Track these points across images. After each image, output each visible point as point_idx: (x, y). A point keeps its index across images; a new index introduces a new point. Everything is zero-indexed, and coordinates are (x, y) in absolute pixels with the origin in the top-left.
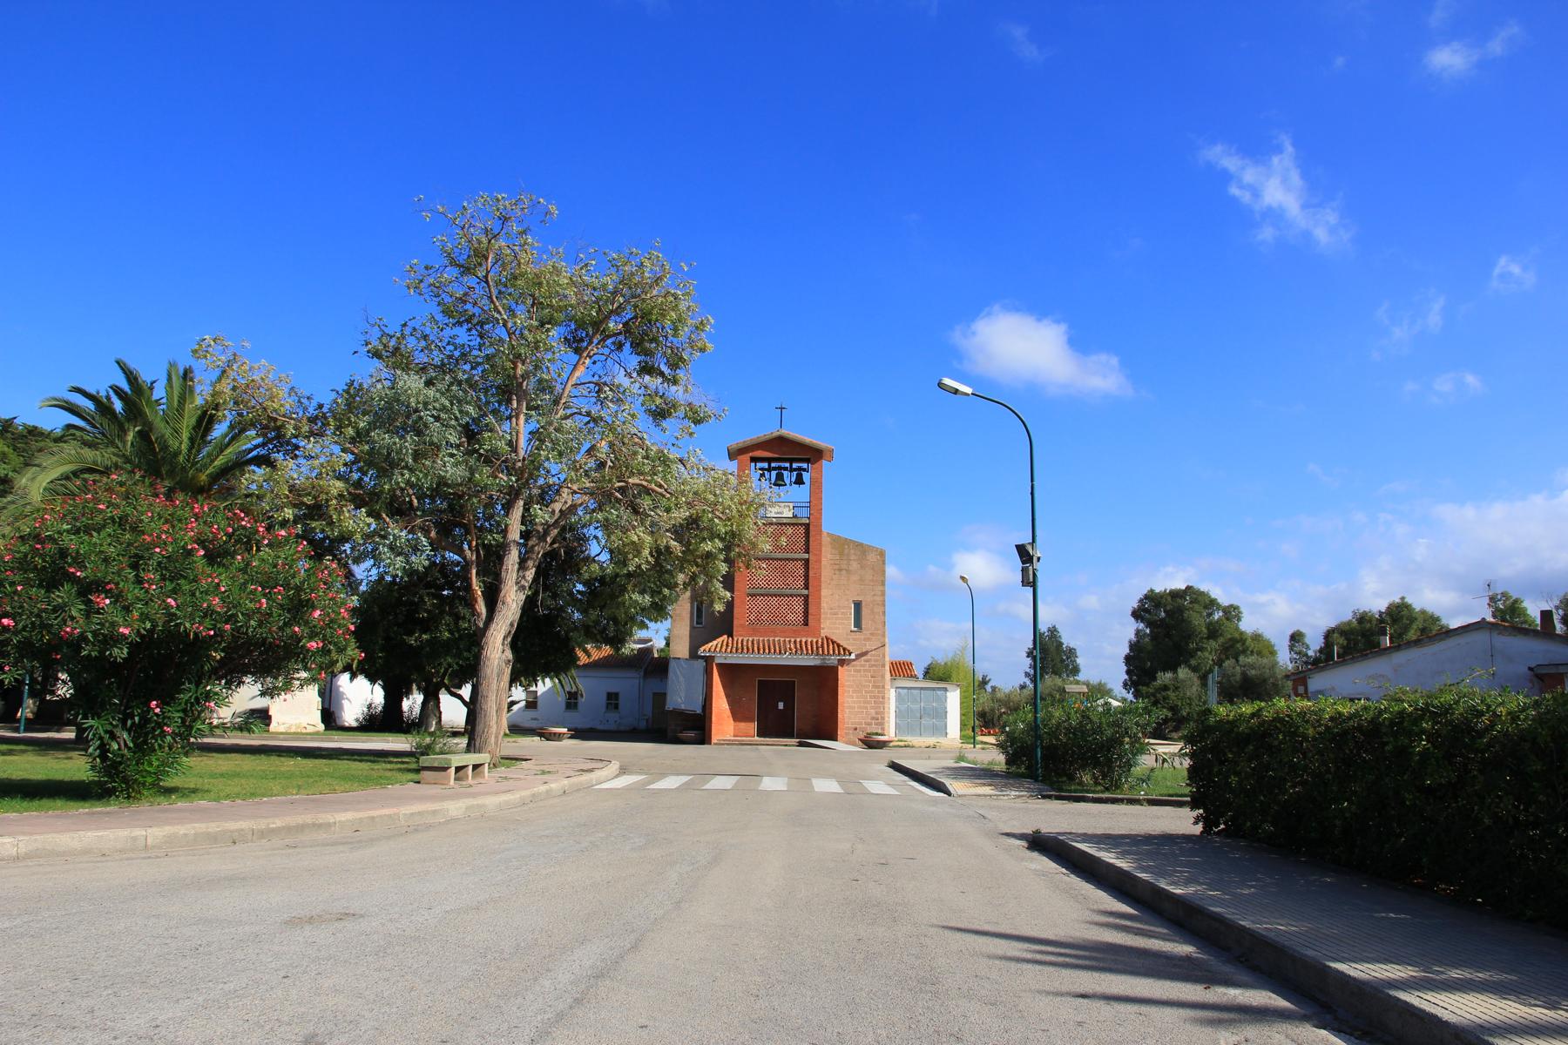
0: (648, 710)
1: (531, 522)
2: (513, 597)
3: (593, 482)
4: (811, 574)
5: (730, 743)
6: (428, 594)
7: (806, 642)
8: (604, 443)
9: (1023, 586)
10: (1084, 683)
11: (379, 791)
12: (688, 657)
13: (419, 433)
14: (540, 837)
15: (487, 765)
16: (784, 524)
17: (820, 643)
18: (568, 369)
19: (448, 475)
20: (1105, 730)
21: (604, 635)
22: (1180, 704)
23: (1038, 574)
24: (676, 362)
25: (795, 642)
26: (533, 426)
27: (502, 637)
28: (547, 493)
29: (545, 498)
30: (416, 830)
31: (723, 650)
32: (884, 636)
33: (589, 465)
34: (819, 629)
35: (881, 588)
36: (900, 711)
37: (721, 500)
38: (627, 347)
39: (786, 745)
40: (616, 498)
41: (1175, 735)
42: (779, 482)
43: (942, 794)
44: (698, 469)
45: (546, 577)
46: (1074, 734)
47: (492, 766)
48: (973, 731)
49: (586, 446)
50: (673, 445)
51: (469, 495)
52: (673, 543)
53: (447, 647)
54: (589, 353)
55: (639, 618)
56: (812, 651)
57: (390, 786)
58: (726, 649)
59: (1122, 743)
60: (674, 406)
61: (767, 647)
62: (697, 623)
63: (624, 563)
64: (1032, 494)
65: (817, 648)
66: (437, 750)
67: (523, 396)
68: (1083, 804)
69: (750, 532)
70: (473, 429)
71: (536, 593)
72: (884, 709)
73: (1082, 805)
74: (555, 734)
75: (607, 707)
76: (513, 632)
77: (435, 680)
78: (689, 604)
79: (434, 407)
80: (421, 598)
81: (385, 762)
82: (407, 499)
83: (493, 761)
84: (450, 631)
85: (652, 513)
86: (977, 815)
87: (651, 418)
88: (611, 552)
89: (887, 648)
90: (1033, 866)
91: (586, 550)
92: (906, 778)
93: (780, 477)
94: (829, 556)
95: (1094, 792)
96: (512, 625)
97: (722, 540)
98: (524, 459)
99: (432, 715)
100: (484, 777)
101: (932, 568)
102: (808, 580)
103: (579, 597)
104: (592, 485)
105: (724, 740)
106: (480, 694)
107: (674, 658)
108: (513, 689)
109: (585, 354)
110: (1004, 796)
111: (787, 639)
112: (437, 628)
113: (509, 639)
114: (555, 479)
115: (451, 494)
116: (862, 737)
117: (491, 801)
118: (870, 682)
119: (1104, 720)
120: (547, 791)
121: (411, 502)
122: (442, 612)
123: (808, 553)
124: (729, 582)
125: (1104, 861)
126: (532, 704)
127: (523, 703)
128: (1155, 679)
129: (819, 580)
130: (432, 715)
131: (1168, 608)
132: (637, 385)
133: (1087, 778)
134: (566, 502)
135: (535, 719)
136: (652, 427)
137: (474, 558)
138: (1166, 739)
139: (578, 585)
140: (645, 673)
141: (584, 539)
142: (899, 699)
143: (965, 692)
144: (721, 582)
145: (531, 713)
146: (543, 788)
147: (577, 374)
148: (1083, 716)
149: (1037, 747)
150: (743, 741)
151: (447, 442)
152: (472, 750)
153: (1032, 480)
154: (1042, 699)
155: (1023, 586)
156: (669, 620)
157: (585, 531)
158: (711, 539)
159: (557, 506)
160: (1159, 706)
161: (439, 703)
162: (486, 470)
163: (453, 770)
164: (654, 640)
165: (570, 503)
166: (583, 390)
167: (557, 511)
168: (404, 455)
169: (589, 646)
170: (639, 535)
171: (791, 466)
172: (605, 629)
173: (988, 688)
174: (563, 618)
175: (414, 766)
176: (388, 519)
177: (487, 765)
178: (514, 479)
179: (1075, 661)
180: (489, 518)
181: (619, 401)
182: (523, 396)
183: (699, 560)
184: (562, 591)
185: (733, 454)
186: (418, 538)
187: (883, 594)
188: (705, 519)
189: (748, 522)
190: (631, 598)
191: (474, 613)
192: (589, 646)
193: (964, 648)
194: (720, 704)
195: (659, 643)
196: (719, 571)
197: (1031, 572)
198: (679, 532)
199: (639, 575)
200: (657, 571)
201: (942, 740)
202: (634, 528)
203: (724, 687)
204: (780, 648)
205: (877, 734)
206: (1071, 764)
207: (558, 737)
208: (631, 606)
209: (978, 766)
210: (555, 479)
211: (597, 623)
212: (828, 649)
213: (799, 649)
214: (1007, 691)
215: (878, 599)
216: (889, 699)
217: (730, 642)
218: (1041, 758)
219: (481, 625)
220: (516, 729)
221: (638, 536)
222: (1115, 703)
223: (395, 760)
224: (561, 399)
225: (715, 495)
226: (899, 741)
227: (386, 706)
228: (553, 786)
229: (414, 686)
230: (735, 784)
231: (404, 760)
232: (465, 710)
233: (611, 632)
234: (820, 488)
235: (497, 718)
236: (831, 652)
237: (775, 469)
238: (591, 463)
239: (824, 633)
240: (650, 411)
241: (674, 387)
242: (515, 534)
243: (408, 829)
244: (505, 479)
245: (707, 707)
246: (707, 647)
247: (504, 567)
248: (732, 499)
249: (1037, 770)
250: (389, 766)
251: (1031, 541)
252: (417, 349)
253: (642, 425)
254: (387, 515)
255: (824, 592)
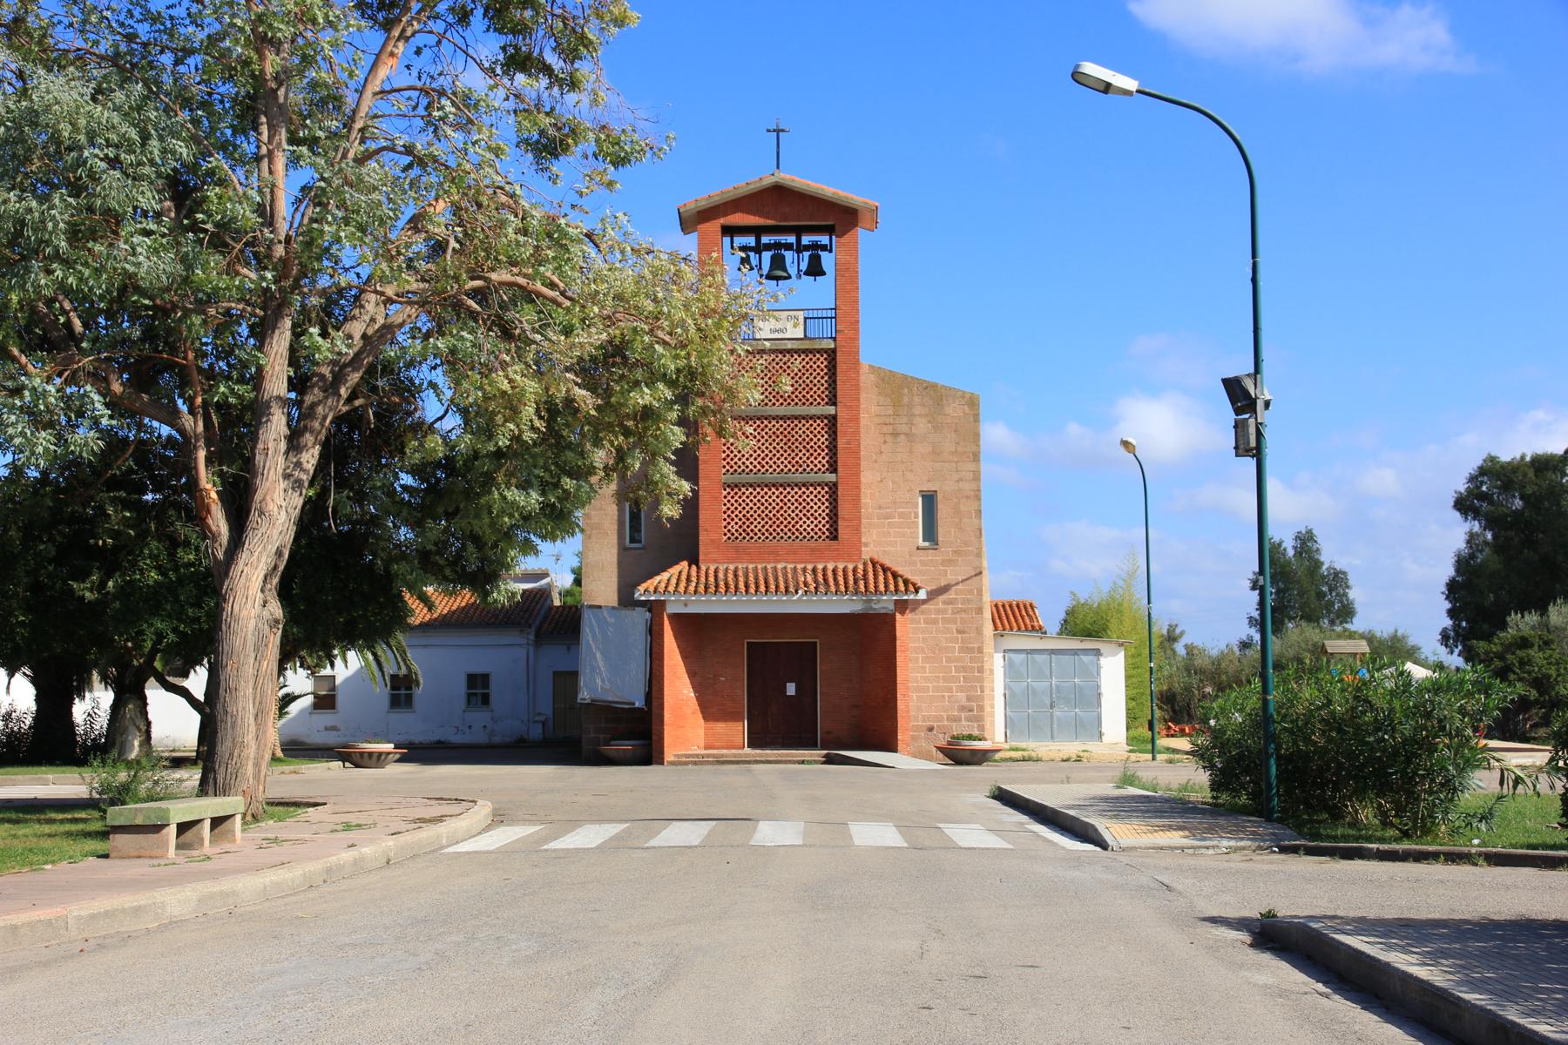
0: (546, 707)
1: (307, 358)
2: (279, 501)
3: (423, 280)
4: (841, 442)
5: (698, 761)
6: (114, 501)
7: (834, 571)
8: (441, 205)
9: (1237, 456)
10: (1362, 637)
11: (26, 877)
12: (615, 604)
13: (76, 189)
14: (341, 948)
15: (238, 818)
16: (789, 351)
17: (860, 571)
18: (366, 61)
19: (142, 272)
20: (1401, 723)
21: (458, 569)
22: (1553, 672)
23: (1266, 433)
24: (575, 45)
25: (814, 570)
26: (305, 175)
27: (261, 577)
28: (336, 303)
29: (333, 311)
30: (101, 947)
31: (682, 588)
32: (979, 555)
33: (415, 248)
34: (857, 545)
35: (971, 466)
36: (1013, 694)
37: (665, 309)
38: (478, 20)
39: (803, 762)
40: (469, 308)
41: (1542, 732)
42: (777, 272)
43: (1089, 847)
44: (623, 252)
45: (342, 462)
46: (1340, 731)
47: (249, 818)
48: (1151, 727)
49: (410, 211)
50: (573, 206)
51: (185, 309)
52: (580, 393)
53: (154, 600)
54: (403, 30)
55: (521, 535)
56: (846, 587)
57: (49, 867)
58: (686, 588)
59: (1432, 749)
60: (573, 131)
61: (762, 582)
62: (632, 540)
63: (489, 432)
64: (1254, 280)
65: (856, 581)
66: (142, 792)
67: (280, 114)
68: (1359, 862)
69: (722, 364)
70: (187, 182)
71: (323, 494)
72: (982, 692)
73: (1358, 865)
74: (370, 754)
75: (469, 702)
76: (281, 568)
77: (135, 662)
78: (615, 507)
79: (107, 140)
80: (101, 510)
81: (39, 821)
82: (62, 320)
83: (253, 809)
84: (159, 569)
85: (538, 337)
86: (1156, 885)
87: (530, 156)
88: (464, 412)
89: (987, 579)
90: (1261, 978)
91: (416, 409)
92: (1024, 818)
93: (778, 262)
94: (874, 409)
95: (1382, 840)
96: (279, 553)
97: (672, 384)
98: (288, 240)
99: (132, 729)
100: (234, 841)
101: (1074, 429)
102: (835, 454)
103: (406, 497)
104: (421, 285)
105: (688, 756)
106: (223, 684)
107: (591, 607)
108: (289, 673)
109: (396, 33)
110: (1207, 848)
111: (800, 566)
112: (134, 564)
113: (276, 581)
114: (351, 276)
115: (147, 308)
116: (942, 743)
117: (248, 885)
118: (955, 640)
119: (1396, 704)
120: (355, 862)
121: (68, 325)
122: (143, 535)
123: (835, 404)
124: (687, 463)
125: (1398, 970)
126: (325, 701)
127: (309, 700)
128: (1503, 626)
129: (856, 453)
130: (132, 729)
131: (1529, 490)
132: (501, 93)
133: (1367, 815)
134: (373, 320)
135: (334, 728)
136: (530, 171)
137: (200, 428)
138: (1527, 741)
139: (403, 475)
140: (538, 635)
141: (410, 391)
142: (1010, 668)
143: (1133, 656)
144: (672, 463)
145: (325, 718)
146: (348, 856)
147: (383, 72)
148: (1356, 698)
149: (1269, 756)
150: (722, 756)
151: (135, 208)
152: (211, 791)
153: (1254, 255)
154: (1278, 666)
155: (1237, 456)
156: (579, 536)
157: (413, 373)
158: (650, 384)
159: (357, 329)
160: (1512, 677)
161: (145, 704)
162: (215, 260)
163: (173, 829)
164: (553, 575)
165: (381, 321)
166: (401, 103)
167: (357, 336)
168: (51, 233)
169: (429, 590)
170: (515, 378)
171: (799, 240)
172: (459, 556)
173: (1180, 648)
174: (378, 538)
175: (97, 826)
176: (24, 359)
177: (238, 818)
178: (269, 275)
179: (1345, 595)
180: (227, 353)
181: (465, 125)
182: (280, 114)
183: (630, 423)
184: (374, 488)
185: (690, 221)
186: (85, 395)
187: (976, 477)
188: (638, 346)
189: (719, 349)
190: (505, 498)
191: (206, 533)
192: (429, 590)
193: (1131, 575)
194: (679, 689)
195: (562, 580)
196: (667, 444)
197: (1252, 430)
198: (588, 371)
199: (516, 455)
200: (550, 446)
201: (1094, 747)
202: (504, 366)
203: (685, 657)
204: (786, 582)
205: (970, 737)
206: (1336, 789)
207: (377, 760)
208: (503, 512)
209: (1160, 793)
210: (351, 276)
211: (442, 546)
212: (876, 583)
213: (823, 583)
214: (1215, 653)
215: (967, 487)
216: (992, 671)
217: (694, 573)
218: (1277, 776)
219: (220, 555)
220: (296, 749)
221: (511, 381)
222: (1419, 673)
223: (60, 816)
224: (354, 121)
225: (655, 300)
226: (1012, 749)
227: (39, 716)
228: (366, 850)
229: (95, 676)
230: (708, 835)
231: (77, 815)
232: (195, 718)
233: (472, 565)
234: (854, 280)
235: (258, 730)
236: (882, 588)
237: (768, 247)
238: (419, 245)
239: (867, 553)
240: (527, 142)
241: (572, 94)
242: (277, 383)
243: (85, 946)
244: (253, 276)
245: (654, 694)
246: (650, 584)
247: (260, 446)
248: (687, 307)
249: (1270, 799)
250: (47, 829)
251: (1252, 370)
252: (60, 22)
253: (516, 169)
254: (22, 351)
255: (867, 477)
